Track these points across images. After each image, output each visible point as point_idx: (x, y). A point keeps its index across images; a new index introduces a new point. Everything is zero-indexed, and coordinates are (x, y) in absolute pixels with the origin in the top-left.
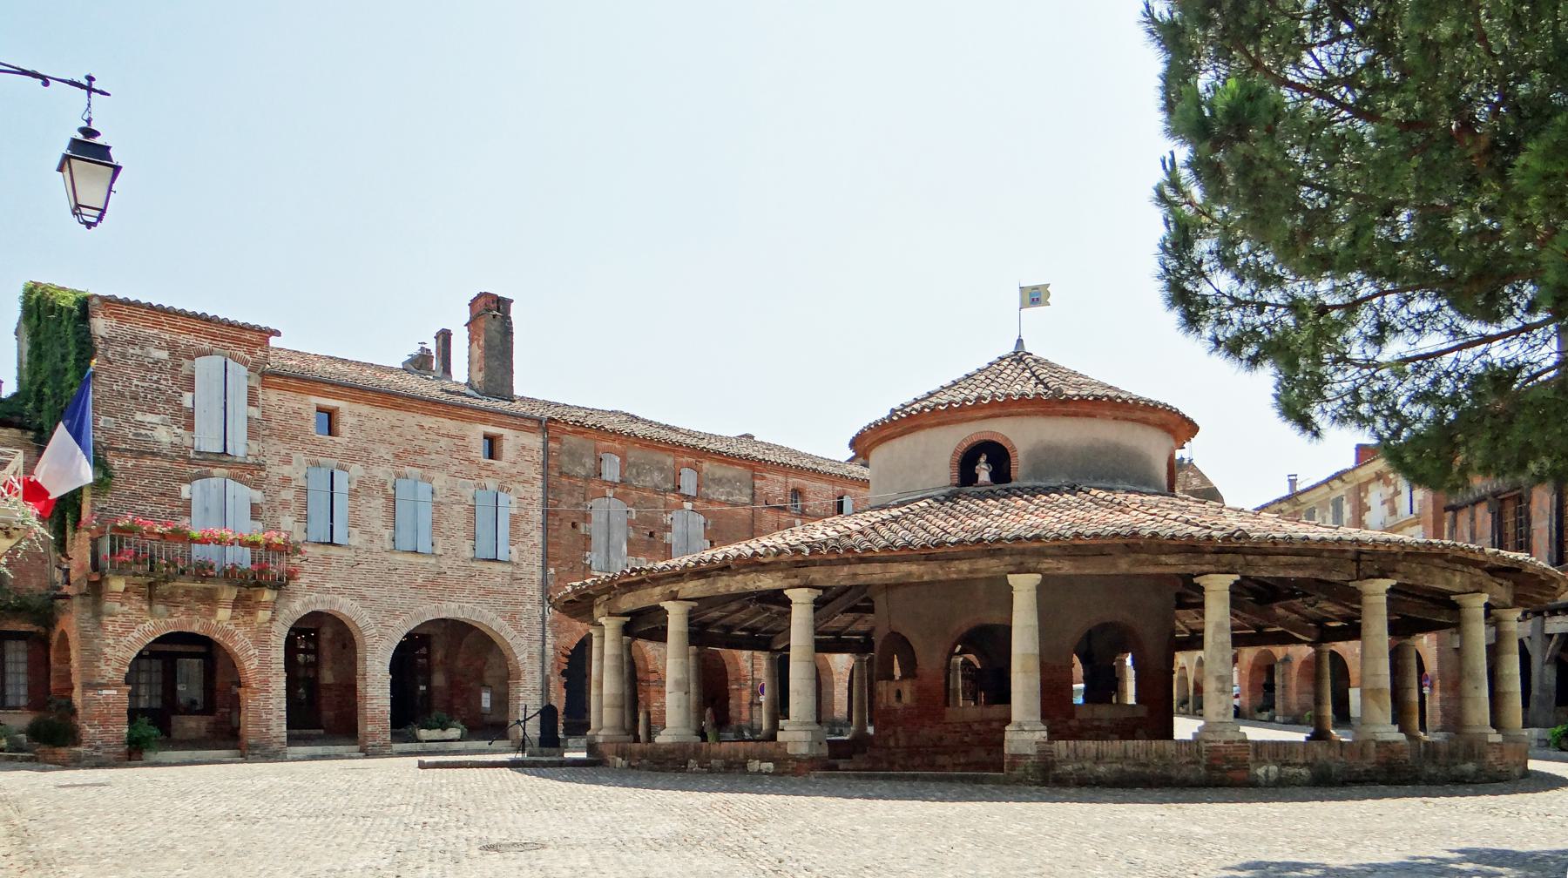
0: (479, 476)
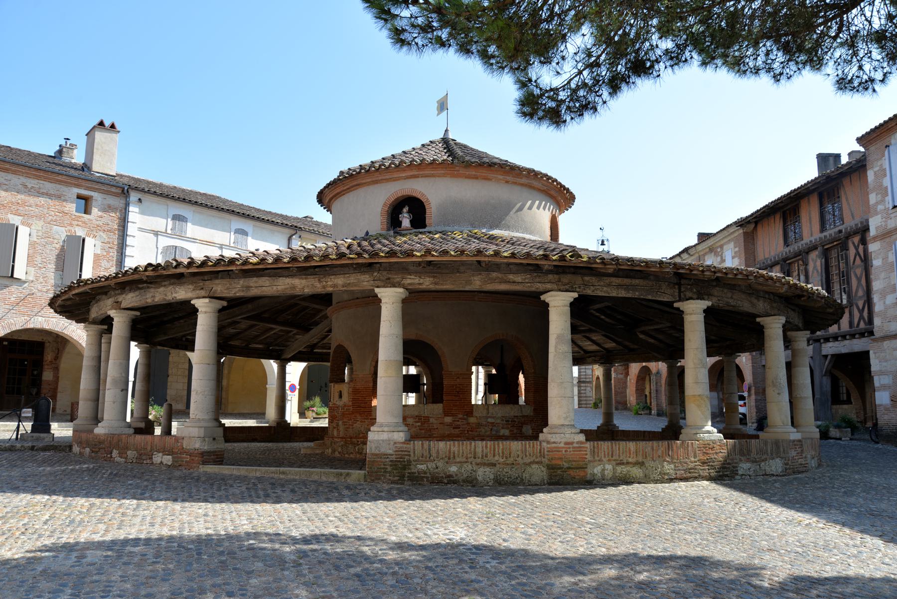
0: (71, 225)
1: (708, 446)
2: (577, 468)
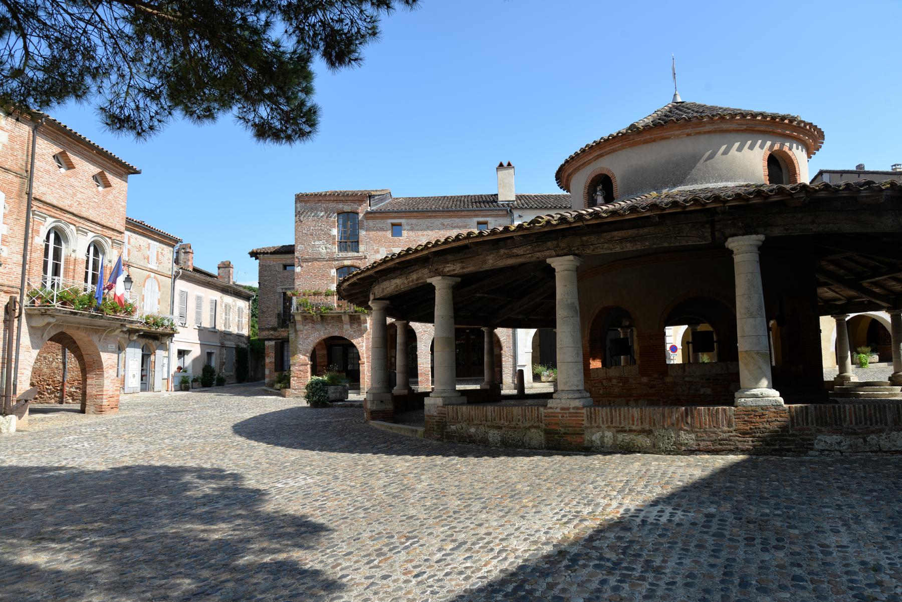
1: (759, 412)
2: (574, 434)
